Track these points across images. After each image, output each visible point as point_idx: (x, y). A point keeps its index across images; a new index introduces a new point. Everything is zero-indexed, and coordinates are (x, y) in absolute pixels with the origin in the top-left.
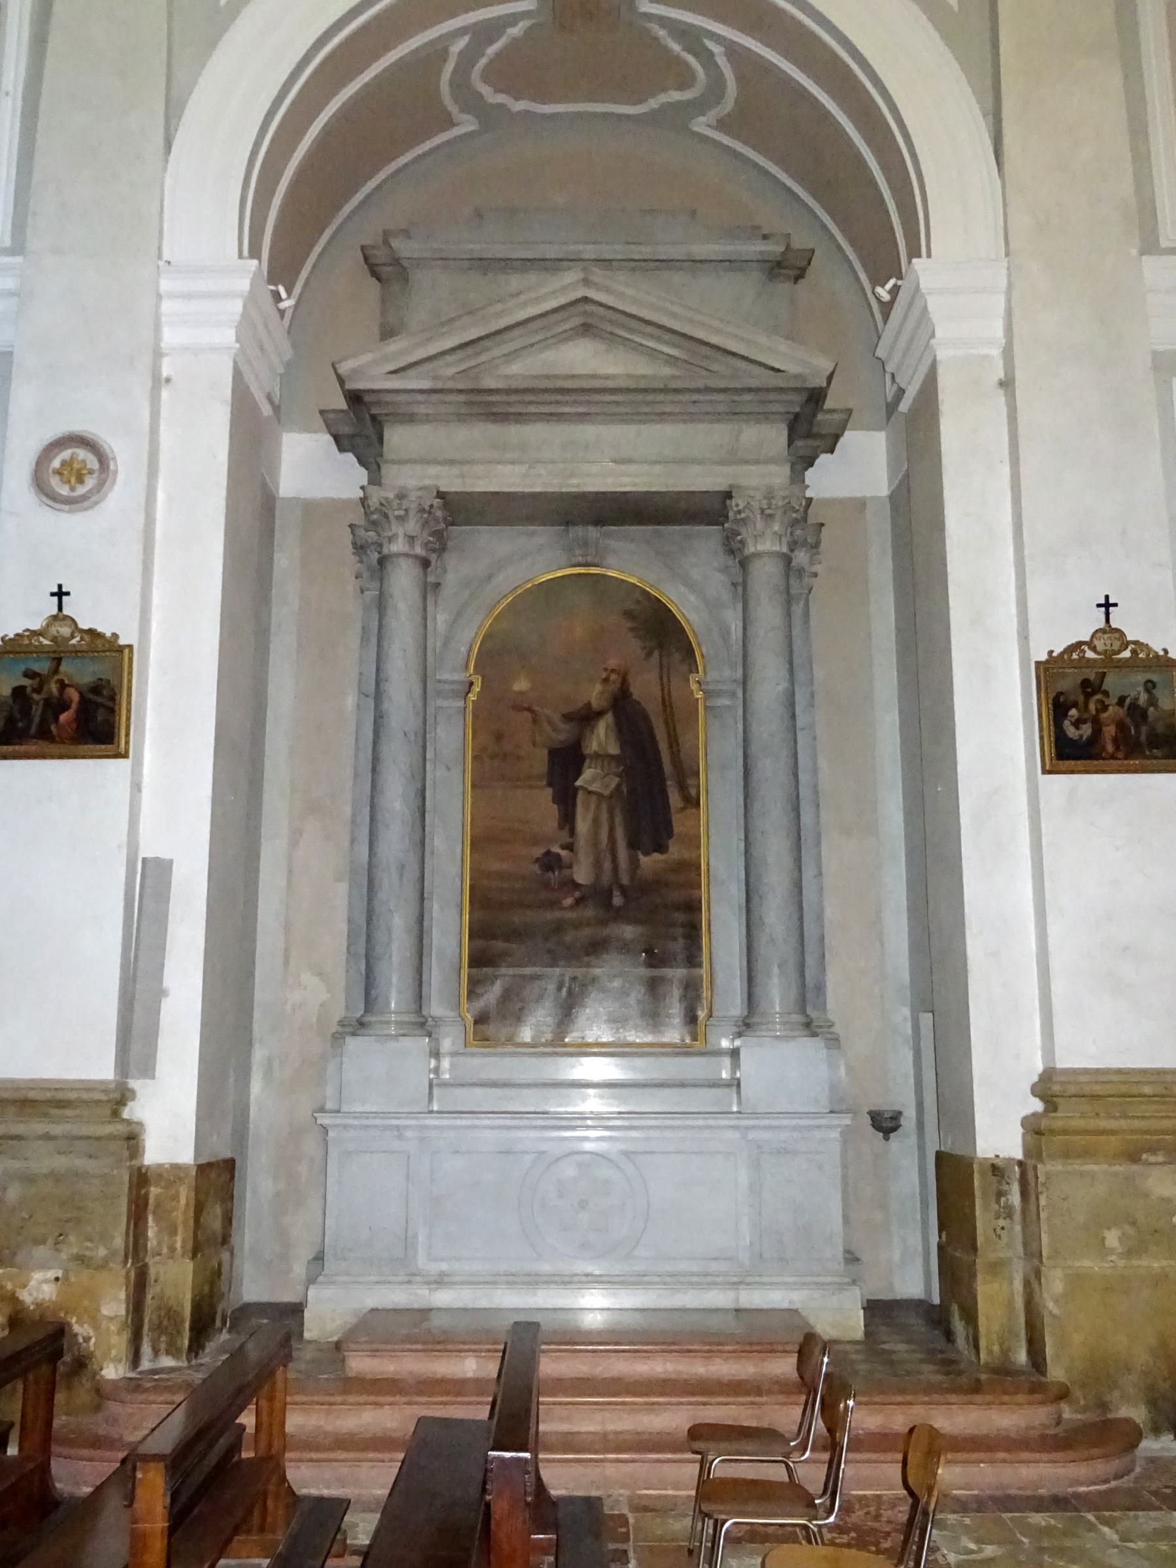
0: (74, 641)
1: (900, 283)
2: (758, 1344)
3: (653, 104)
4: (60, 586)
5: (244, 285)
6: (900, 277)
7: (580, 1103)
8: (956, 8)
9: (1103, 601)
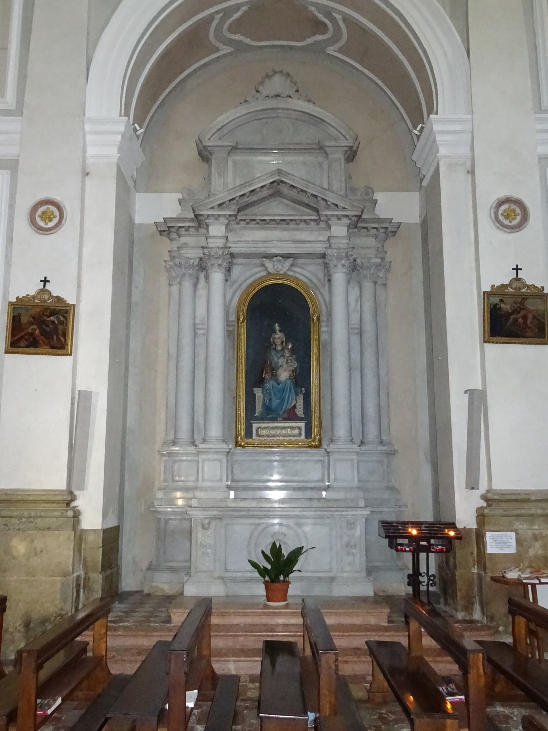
0: (49, 301)
1: (423, 126)
2: (252, 241)
3: (309, 41)
4: (45, 278)
5: (122, 128)
9: (515, 267)
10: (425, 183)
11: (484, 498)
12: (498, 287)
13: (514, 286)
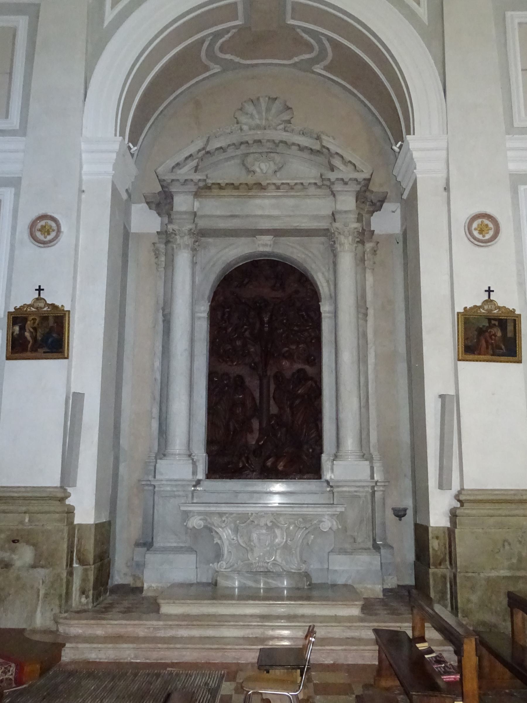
0: (45, 309)
3: (296, 59)
4: (40, 286)
5: (116, 147)
6: (403, 142)
7: (159, 589)
8: (427, 24)
9: (38, 288)
10: (405, 196)
11: (457, 497)
12: (471, 308)
13: (486, 307)
